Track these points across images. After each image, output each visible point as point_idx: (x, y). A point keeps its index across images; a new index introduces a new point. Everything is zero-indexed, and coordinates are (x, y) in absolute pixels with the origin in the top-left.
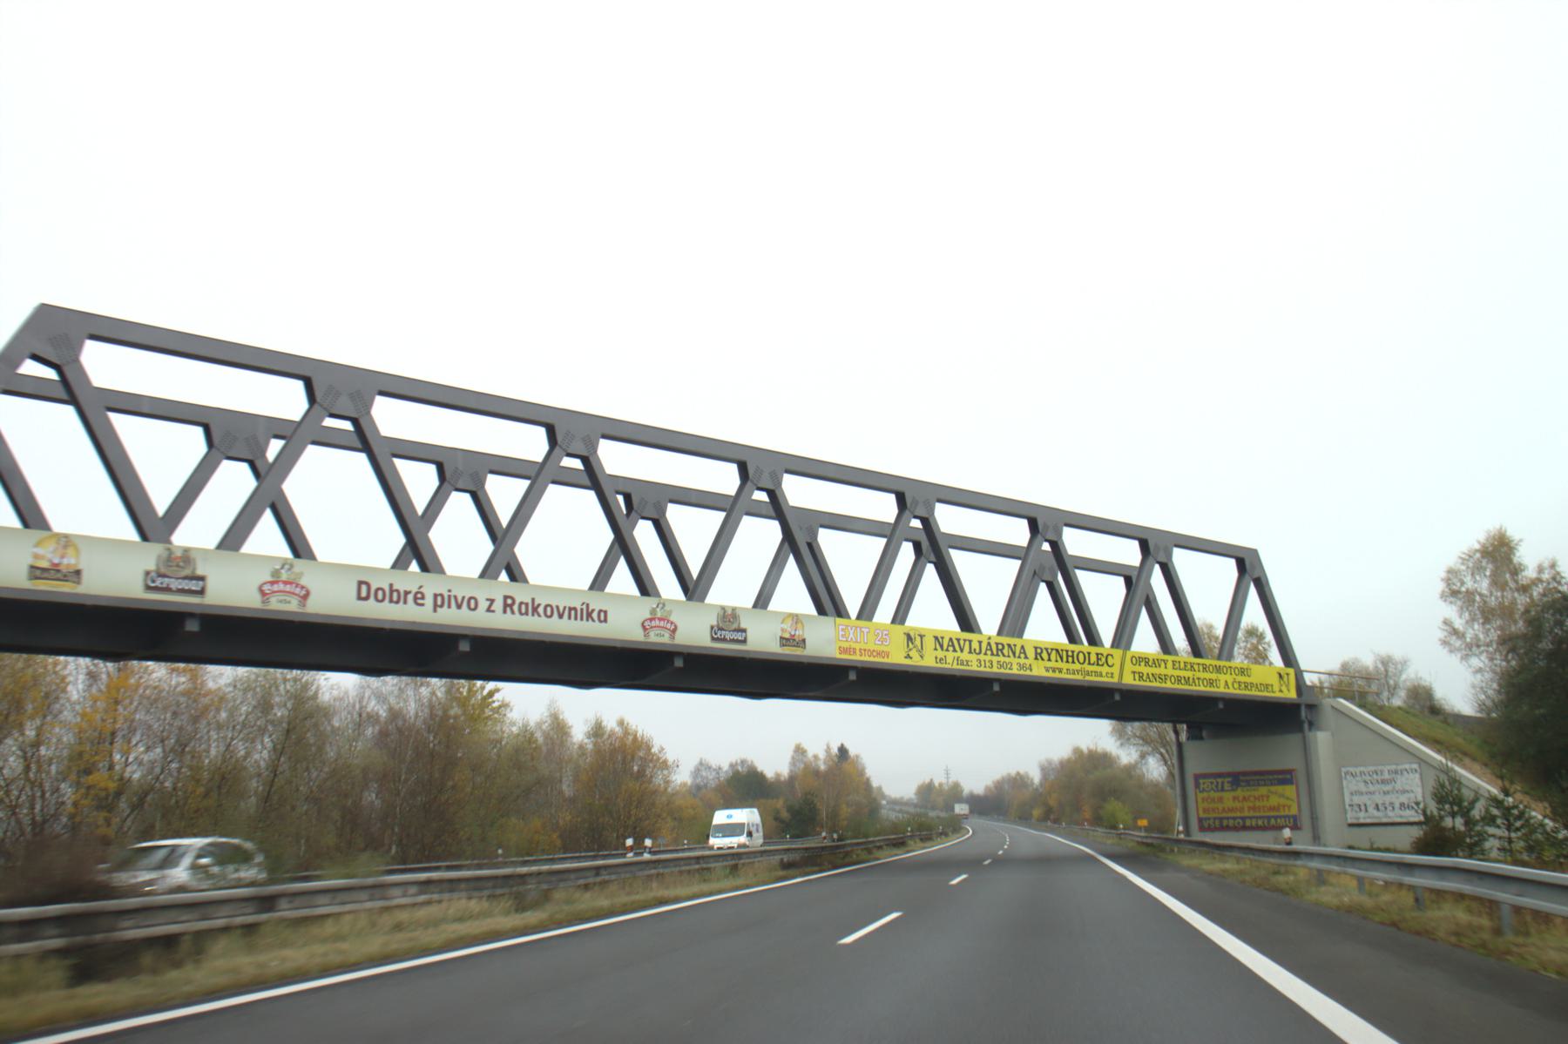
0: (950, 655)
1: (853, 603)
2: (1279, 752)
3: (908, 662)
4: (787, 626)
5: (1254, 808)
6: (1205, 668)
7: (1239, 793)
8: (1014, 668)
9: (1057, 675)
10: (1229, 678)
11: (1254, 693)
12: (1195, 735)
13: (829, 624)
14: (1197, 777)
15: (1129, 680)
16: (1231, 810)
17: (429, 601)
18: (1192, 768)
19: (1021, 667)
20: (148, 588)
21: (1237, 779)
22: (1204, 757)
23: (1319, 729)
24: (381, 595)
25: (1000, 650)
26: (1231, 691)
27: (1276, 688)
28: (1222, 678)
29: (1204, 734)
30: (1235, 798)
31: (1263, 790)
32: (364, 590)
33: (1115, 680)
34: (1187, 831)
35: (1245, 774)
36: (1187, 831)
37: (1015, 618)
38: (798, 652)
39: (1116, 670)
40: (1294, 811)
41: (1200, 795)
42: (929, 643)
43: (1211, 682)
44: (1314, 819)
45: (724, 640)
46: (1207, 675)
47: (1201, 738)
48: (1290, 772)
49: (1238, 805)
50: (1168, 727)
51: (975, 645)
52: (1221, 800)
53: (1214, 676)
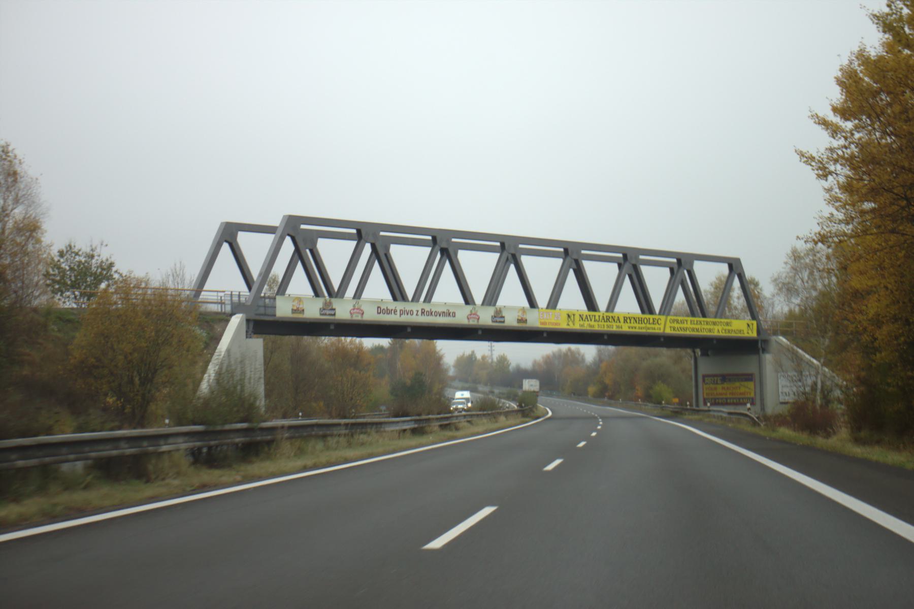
0: (586, 323)
1: (410, 296)
2: (748, 365)
3: (568, 327)
4: (295, 303)
5: (732, 394)
6: (707, 323)
7: (725, 385)
8: (614, 328)
9: (634, 330)
10: (720, 328)
11: (733, 335)
12: (705, 354)
13: (400, 306)
14: (704, 376)
15: (668, 331)
16: (721, 394)
17: (398, 313)
18: (702, 371)
19: (618, 327)
20: (321, 314)
21: (725, 378)
22: (707, 366)
23: (768, 352)
24: (388, 311)
25: (608, 320)
26: (721, 334)
27: (745, 332)
28: (716, 328)
29: (709, 353)
30: (723, 388)
31: (737, 384)
32: (380, 311)
33: (662, 331)
34: (697, 405)
35: (730, 375)
36: (691, 405)
37: (492, 295)
38: (300, 316)
39: (662, 327)
40: (752, 395)
41: (705, 386)
42: (577, 317)
43: (710, 330)
44: (762, 400)
45: (325, 314)
46: (709, 327)
47: (708, 355)
48: (751, 375)
49: (724, 391)
50: (689, 351)
51: (597, 318)
52: (716, 389)
53: (712, 327)
